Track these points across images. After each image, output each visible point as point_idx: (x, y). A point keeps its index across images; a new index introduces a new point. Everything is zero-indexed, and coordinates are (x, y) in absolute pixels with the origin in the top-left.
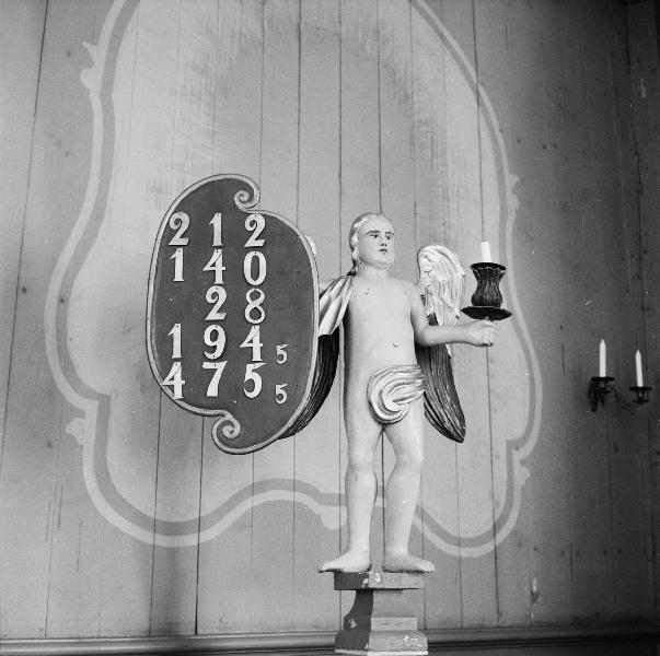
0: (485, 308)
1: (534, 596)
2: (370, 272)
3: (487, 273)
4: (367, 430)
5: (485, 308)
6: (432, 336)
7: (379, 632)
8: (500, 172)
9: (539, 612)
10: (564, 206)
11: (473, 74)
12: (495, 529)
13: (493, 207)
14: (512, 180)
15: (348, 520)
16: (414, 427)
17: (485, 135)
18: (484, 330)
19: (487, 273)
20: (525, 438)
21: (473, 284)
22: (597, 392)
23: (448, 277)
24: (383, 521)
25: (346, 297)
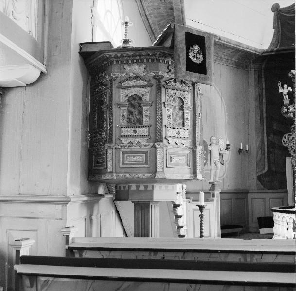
0: (228, 149)
1: (229, 186)
2: (213, 144)
3: (228, 145)
4: (213, 165)
5: (228, 149)
6: (221, 152)
7: (159, 172)
8: (225, 112)
9: (230, 188)
10: (236, 117)
11: (220, 94)
12: (223, 175)
13: (224, 120)
14: (227, 114)
15: (252, 206)
16: (219, 165)
17: (223, 106)
18: (228, 152)
19: (228, 145)
20: (228, 160)
21: (226, 146)
22: (240, 151)
23: (223, 146)
24: (215, 175)
25: (211, 148)
